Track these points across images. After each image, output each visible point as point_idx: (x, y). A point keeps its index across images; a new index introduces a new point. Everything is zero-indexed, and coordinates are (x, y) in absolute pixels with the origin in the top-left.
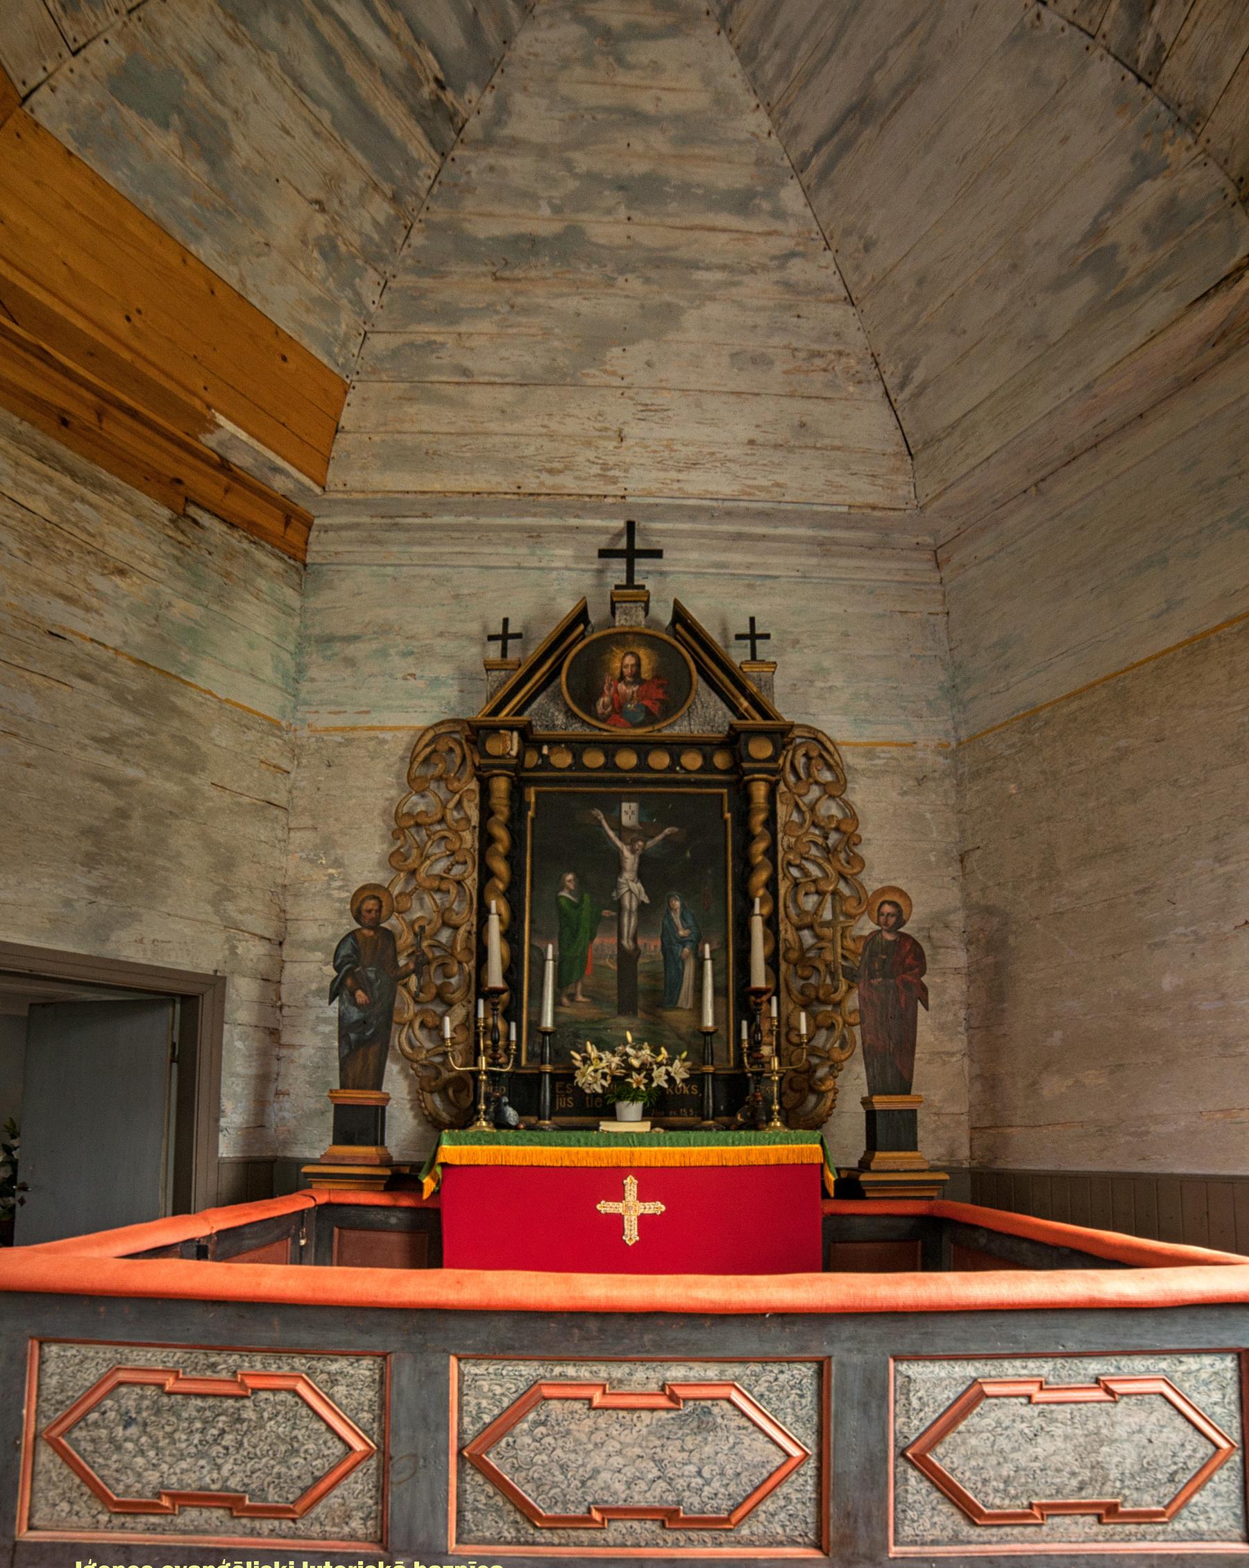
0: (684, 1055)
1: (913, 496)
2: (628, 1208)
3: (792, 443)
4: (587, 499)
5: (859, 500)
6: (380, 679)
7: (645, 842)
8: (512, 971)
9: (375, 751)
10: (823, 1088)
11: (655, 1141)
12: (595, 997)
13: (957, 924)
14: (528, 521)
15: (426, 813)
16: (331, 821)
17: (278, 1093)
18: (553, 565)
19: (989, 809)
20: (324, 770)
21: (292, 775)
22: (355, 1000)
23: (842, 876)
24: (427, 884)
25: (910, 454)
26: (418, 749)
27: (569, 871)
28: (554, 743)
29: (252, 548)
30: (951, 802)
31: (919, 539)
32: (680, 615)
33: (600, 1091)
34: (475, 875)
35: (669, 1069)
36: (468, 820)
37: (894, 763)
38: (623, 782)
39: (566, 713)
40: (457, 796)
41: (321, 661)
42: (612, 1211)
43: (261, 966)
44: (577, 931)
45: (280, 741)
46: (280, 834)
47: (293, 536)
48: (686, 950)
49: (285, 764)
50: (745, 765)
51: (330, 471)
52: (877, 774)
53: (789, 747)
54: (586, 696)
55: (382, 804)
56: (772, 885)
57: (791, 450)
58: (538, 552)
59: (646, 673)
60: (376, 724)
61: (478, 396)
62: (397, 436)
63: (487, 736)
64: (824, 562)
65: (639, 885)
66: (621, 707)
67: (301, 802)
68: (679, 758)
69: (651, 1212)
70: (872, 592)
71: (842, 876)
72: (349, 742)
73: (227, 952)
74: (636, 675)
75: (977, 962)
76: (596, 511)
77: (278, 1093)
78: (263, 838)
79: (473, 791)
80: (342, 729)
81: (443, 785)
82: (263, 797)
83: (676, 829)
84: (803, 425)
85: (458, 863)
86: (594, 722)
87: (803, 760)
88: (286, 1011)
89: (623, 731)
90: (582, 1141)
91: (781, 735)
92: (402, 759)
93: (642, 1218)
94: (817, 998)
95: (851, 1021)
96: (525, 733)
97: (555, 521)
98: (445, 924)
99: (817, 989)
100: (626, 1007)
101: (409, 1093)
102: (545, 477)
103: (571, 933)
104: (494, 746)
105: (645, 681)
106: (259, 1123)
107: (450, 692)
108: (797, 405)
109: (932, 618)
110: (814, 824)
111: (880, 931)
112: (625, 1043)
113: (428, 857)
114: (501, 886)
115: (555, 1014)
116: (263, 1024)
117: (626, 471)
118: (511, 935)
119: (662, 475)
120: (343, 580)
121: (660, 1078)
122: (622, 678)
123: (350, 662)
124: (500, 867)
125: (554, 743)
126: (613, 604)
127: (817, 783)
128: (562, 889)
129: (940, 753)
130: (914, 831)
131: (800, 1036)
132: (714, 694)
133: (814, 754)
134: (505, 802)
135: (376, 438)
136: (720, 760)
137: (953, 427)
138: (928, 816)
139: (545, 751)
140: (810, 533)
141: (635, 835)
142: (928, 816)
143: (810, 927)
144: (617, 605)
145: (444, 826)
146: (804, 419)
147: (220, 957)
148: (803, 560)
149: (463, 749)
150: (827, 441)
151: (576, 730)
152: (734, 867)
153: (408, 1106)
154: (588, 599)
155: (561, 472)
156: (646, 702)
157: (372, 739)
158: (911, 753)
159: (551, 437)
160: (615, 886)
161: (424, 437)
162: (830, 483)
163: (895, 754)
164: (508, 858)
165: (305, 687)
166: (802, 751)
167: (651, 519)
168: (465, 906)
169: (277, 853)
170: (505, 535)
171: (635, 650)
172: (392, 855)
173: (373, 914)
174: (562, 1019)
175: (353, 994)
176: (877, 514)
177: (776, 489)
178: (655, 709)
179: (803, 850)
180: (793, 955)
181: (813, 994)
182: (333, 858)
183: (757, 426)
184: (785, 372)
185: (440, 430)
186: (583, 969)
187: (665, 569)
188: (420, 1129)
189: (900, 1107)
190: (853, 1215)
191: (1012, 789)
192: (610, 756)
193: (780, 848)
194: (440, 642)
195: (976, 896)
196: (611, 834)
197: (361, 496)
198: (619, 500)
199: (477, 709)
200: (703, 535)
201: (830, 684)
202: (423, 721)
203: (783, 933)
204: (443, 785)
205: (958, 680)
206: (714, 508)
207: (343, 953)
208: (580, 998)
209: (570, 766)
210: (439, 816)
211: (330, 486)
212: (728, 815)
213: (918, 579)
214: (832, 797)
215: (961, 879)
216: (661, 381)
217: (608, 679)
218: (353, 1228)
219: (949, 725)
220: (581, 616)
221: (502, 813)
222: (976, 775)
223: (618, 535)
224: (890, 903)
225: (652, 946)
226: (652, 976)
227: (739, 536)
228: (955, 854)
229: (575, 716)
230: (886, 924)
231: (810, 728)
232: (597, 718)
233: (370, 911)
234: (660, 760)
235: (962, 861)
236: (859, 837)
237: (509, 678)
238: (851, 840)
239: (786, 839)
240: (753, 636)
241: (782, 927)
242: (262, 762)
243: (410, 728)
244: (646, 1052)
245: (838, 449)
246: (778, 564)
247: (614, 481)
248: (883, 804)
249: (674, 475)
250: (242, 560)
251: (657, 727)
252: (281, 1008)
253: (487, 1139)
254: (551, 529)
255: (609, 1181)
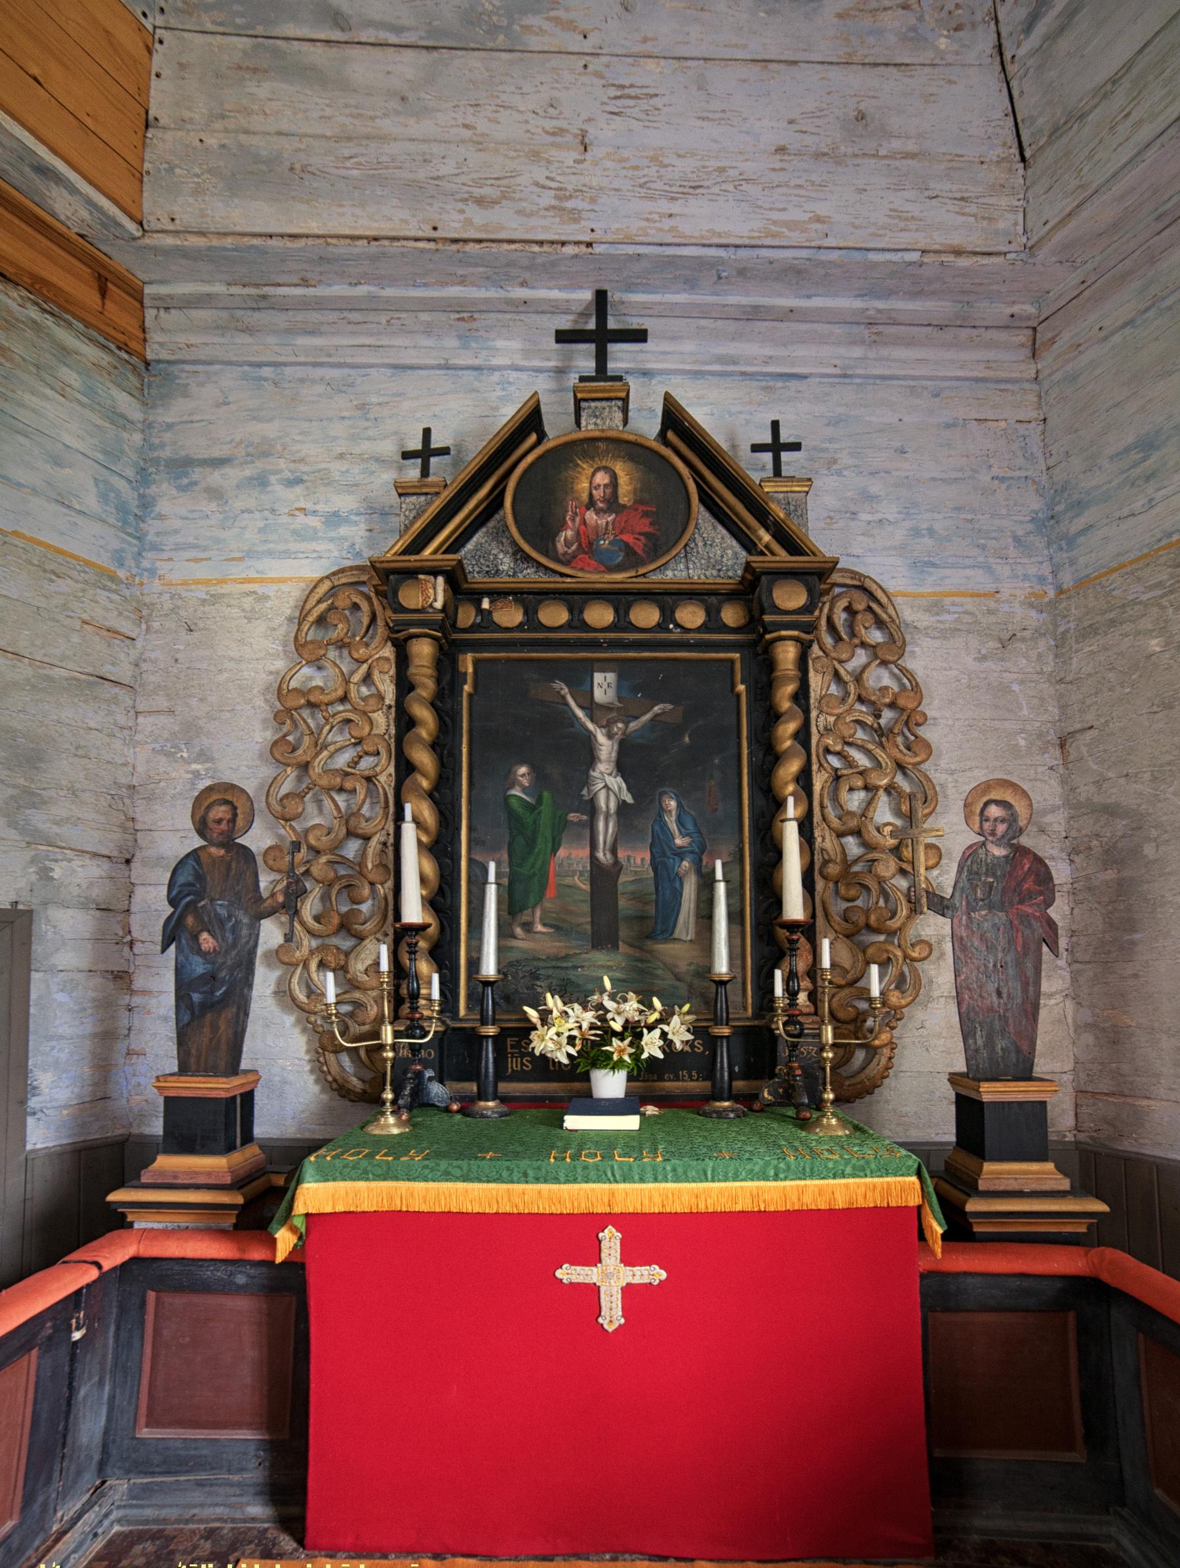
0: (686, 1008)
1: (1020, 229)
2: (607, 1276)
3: (843, 149)
4: (536, 248)
5: (939, 240)
6: (257, 515)
7: (627, 724)
8: (440, 900)
9: (253, 610)
10: (877, 1042)
11: (649, 1175)
12: (559, 928)
13: (1056, 827)
14: (454, 291)
15: (321, 689)
16: (194, 702)
17: (129, 1053)
18: (495, 362)
19: (1111, 676)
20: (184, 635)
21: (139, 643)
22: (199, 945)
23: (900, 767)
24: (324, 782)
25: (1023, 159)
26: (308, 607)
27: (522, 763)
28: (496, 594)
29: (49, 321)
30: (1048, 669)
31: (1016, 309)
32: (674, 419)
33: (565, 1061)
34: (391, 769)
35: (666, 1028)
36: (382, 698)
37: (967, 619)
38: (594, 645)
39: (514, 554)
40: (365, 667)
41: (174, 492)
42: (580, 1280)
43: (95, 892)
44: (534, 841)
45: (114, 597)
46: (122, 719)
47: (118, 313)
48: (685, 864)
49: (126, 627)
50: (767, 618)
51: (145, 194)
52: (945, 634)
53: (825, 599)
54: (540, 528)
55: (263, 679)
56: (804, 779)
57: (839, 160)
58: (473, 345)
59: (624, 499)
60: (253, 574)
61: (363, 67)
62: (243, 138)
63: (399, 583)
64: (872, 354)
65: (619, 779)
66: (590, 544)
67: (152, 678)
68: (673, 612)
69: (646, 1280)
70: (937, 395)
71: (900, 767)
72: (215, 599)
73: (34, 878)
74: (612, 503)
75: (1088, 878)
76: (548, 271)
77: (129, 1053)
78: (92, 724)
79: (387, 659)
80: (207, 582)
81: (345, 652)
82: (90, 670)
83: (669, 707)
84: (861, 117)
85: (367, 753)
86: (552, 565)
87: (844, 616)
88: (138, 948)
89: (594, 577)
90: (531, 1173)
91: (817, 576)
92: (290, 619)
93: (629, 1291)
94: (868, 926)
95: (915, 955)
96: (455, 579)
97: (492, 293)
98: (351, 834)
99: (867, 912)
100: (603, 938)
101: (308, 1052)
102: (472, 211)
103: (525, 845)
104: (411, 597)
105: (624, 506)
106: (99, 1095)
107: (356, 532)
108: (855, 79)
109: (1021, 428)
110: (860, 699)
111: (984, 844)
112: (602, 990)
113: (325, 747)
114: (425, 784)
115: (500, 950)
116: (102, 967)
117: (593, 200)
118: (440, 848)
119: (648, 206)
120: (201, 385)
121: (652, 1046)
122: (591, 504)
123: (215, 494)
124: (423, 758)
125: (496, 594)
126: (578, 402)
127: (863, 645)
128: (512, 787)
129: (1031, 605)
130: (997, 707)
131: (870, 1000)
132: (720, 528)
133: (860, 606)
134: (429, 672)
135: (212, 141)
136: (731, 615)
137: (1114, 81)
138: (1015, 687)
139: (486, 604)
140: (858, 304)
141: (614, 714)
142: (1015, 687)
143: (858, 833)
144: (584, 404)
145: (349, 707)
146: (862, 107)
147: (22, 883)
148: (842, 351)
149: (371, 604)
150: (896, 144)
151: (529, 576)
152: (750, 754)
153: (308, 1068)
154: (543, 399)
155: (495, 202)
156: (628, 538)
157: (247, 594)
158: (993, 605)
159: (480, 143)
160: (586, 781)
161: (284, 142)
162: (895, 213)
163: (969, 607)
164: (435, 746)
165: (152, 527)
166: (843, 603)
167: (630, 288)
168: (379, 810)
169: (117, 744)
170: (424, 317)
171: (609, 464)
172: (275, 743)
173: (224, 826)
174: (513, 956)
175: (195, 938)
176: (964, 262)
177: (818, 226)
178: (639, 547)
179: (846, 733)
180: (833, 869)
181: (862, 921)
182: (197, 749)
183: (791, 122)
184: (840, 16)
185: (309, 131)
186: (543, 887)
187: (649, 366)
188: (324, 1097)
189: (1021, 1098)
190: (965, 1273)
191: (1155, 645)
192: (576, 611)
193: (814, 730)
194: (342, 466)
195: (1086, 791)
196: (580, 713)
197: (200, 242)
198: (583, 248)
199: (389, 547)
200: (704, 312)
201: (878, 516)
202: (314, 570)
203: (819, 840)
204: (345, 652)
205: (1059, 508)
206: (721, 261)
207: (181, 880)
208: (539, 928)
209: (521, 625)
210: (340, 693)
211: (151, 223)
212: (741, 688)
213: (1003, 375)
214: (884, 663)
215: (1061, 770)
216: (645, 40)
217: (571, 505)
218: (180, 1289)
219: (1046, 570)
220: (531, 421)
221: (424, 686)
222: (1088, 632)
223: (583, 315)
224: (997, 803)
225: (638, 860)
226: (639, 897)
227: (754, 314)
228: (1052, 737)
229: (527, 558)
230: (993, 833)
231: (854, 574)
232: (558, 560)
233: (219, 821)
234: (646, 616)
235: (1062, 746)
236: (925, 715)
237: (429, 504)
238: (911, 719)
239: (822, 718)
240: (776, 447)
241: (817, 833)
242: (85, 622)
243: (300, 579)
244: (632, 1007)
245: (913, 156)
246: (808, 357)
247: (575, 216)
248: (954, 673)
249: (664, 206)
250: (29, 334)
251: (642, 571)
252: (131, 944)
253: (379, 1171)
254: (489, 307)
255: (578, 1236)
